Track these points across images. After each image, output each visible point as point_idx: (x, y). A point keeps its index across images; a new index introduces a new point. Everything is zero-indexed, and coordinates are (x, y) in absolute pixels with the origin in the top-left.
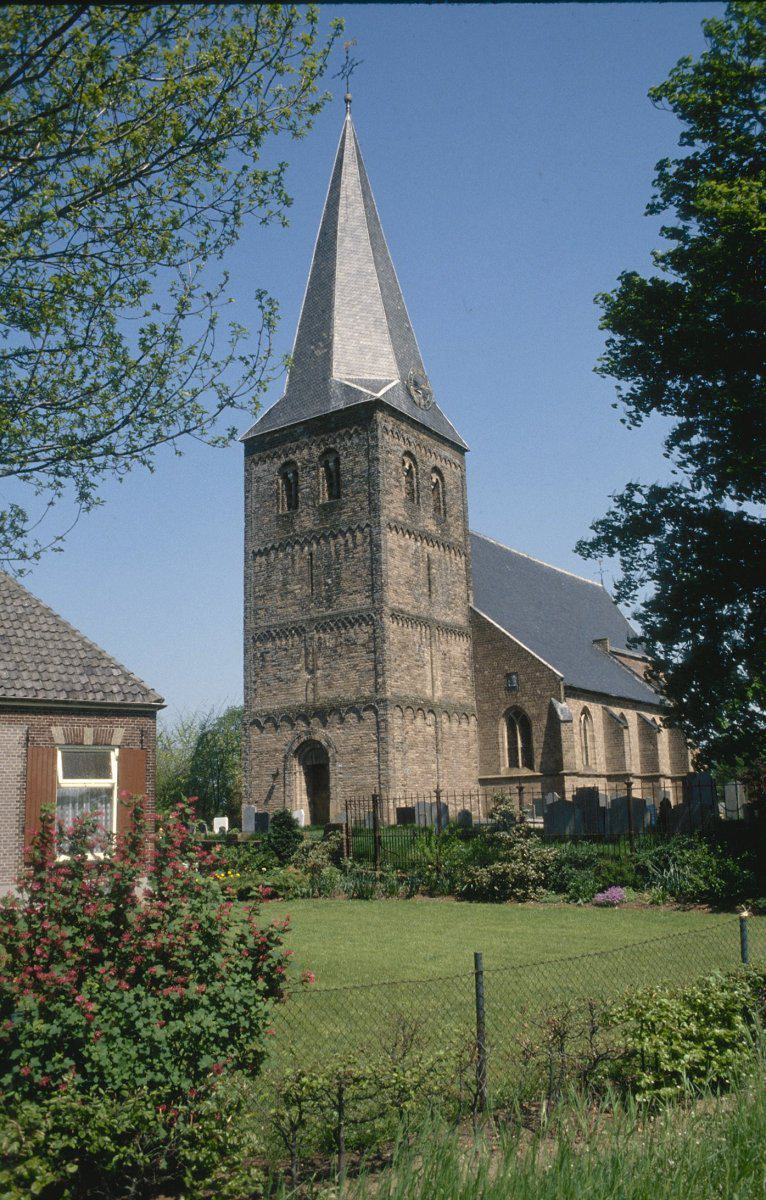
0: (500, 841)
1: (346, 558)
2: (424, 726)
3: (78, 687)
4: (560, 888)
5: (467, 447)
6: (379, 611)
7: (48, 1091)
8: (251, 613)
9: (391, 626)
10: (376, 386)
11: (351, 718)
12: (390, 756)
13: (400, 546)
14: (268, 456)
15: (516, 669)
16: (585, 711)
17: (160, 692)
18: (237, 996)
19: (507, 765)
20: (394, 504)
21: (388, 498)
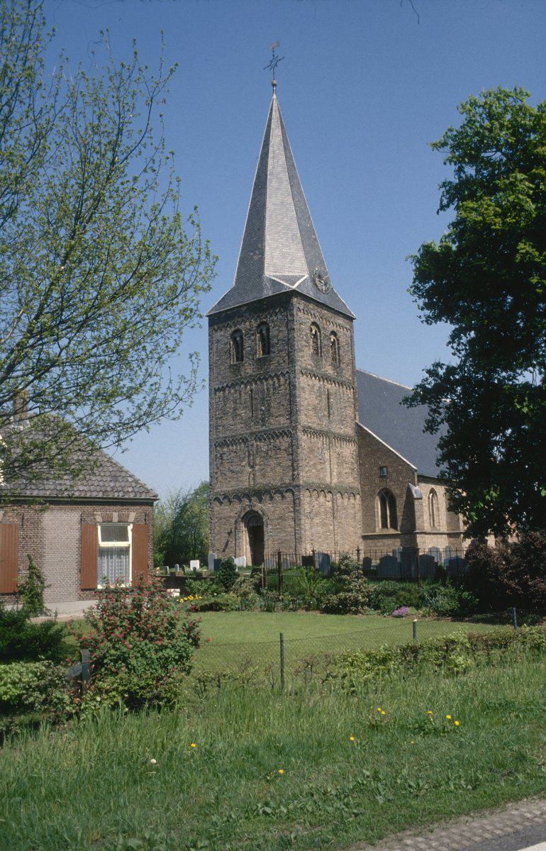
0: (345, 580)
1: (274, 393)
2: (325, 502)
3: (109, 489)
4: (377, 607)
5: (355, 316)
6: (295, 428)
7: (117, 673)
8: (214, 428)
9: (303, 438)
10: (292, 280)
11: (277, 497)
12: (303, 521)
13: (308, 385)
14: (224, 326)
15: (386, 464)
16: (432, 491)
17: (157, 492)
18: (182, 644)
19: (380, 527)
20: (304, 357)
21: (300, 354)
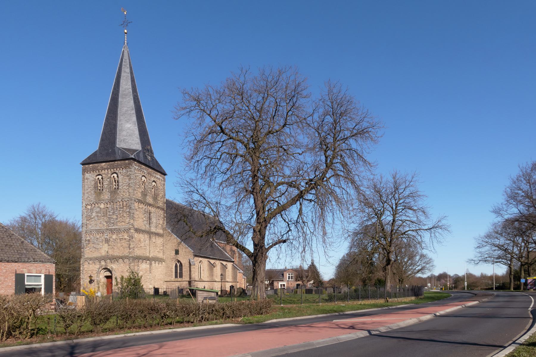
5: (167, 172)
11: (121, 260)
19: (174, 277)
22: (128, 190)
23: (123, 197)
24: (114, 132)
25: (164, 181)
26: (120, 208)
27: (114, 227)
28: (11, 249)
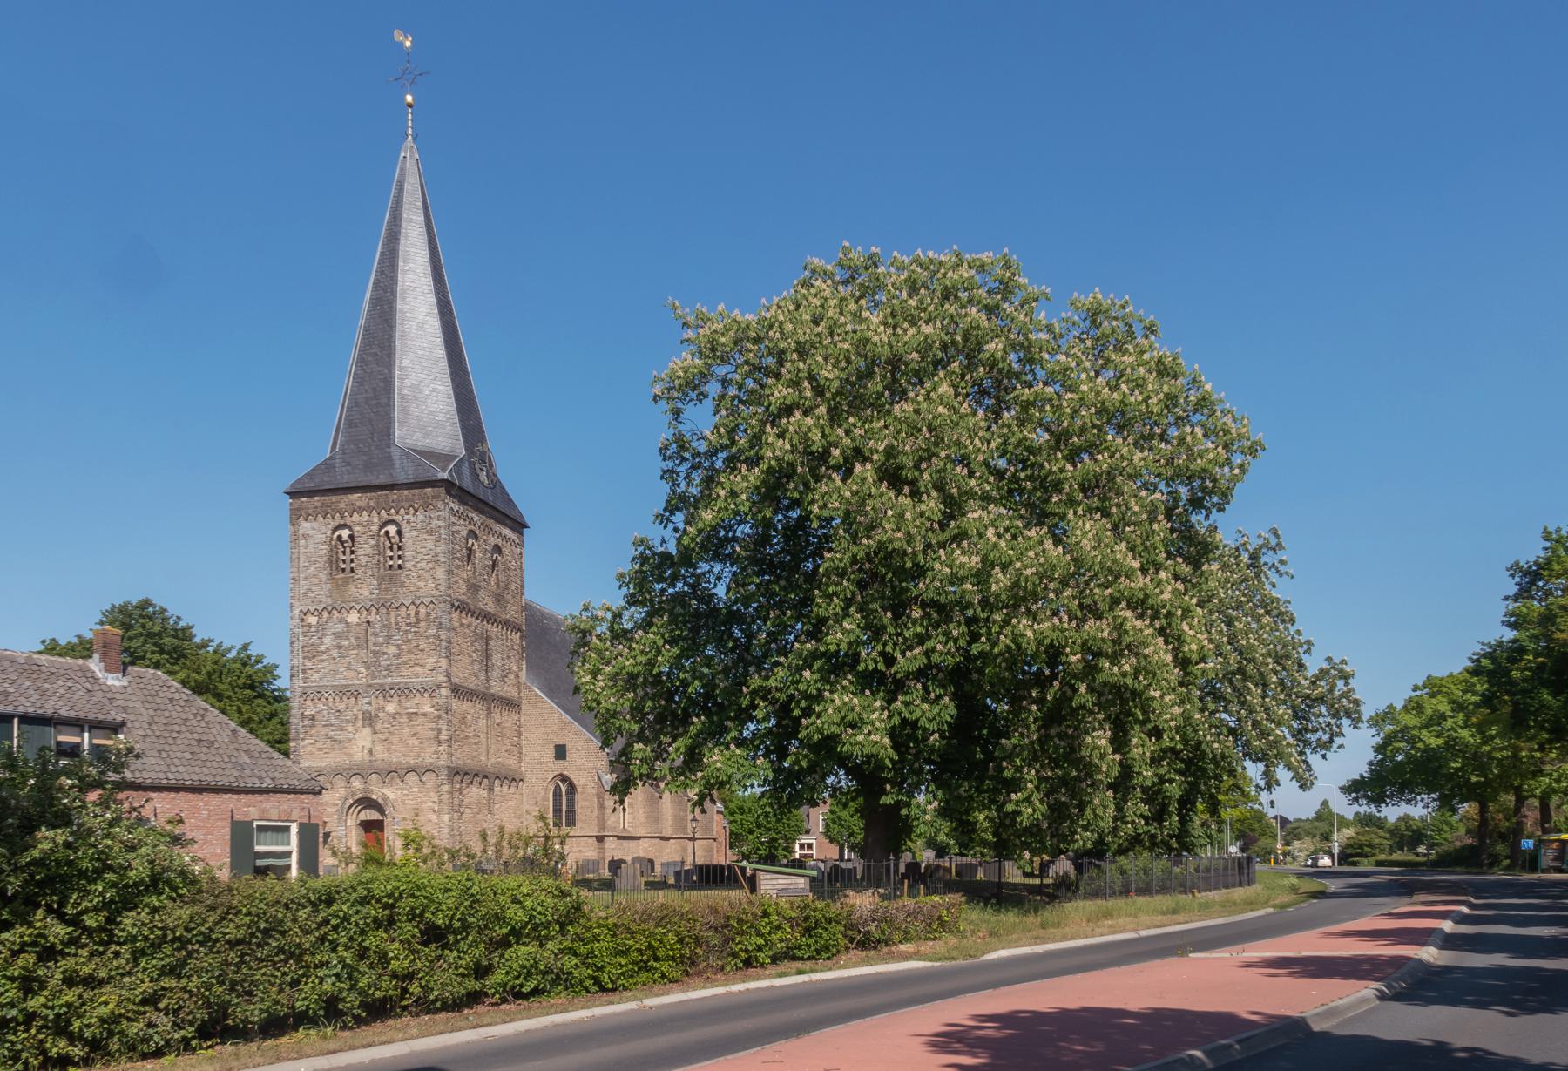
22: (432, 572)
23: (418, 594)
24: (385, 401)
25: (521, 545)
26: (407, 625)
27: (389, 680)
28: (213, 751)
